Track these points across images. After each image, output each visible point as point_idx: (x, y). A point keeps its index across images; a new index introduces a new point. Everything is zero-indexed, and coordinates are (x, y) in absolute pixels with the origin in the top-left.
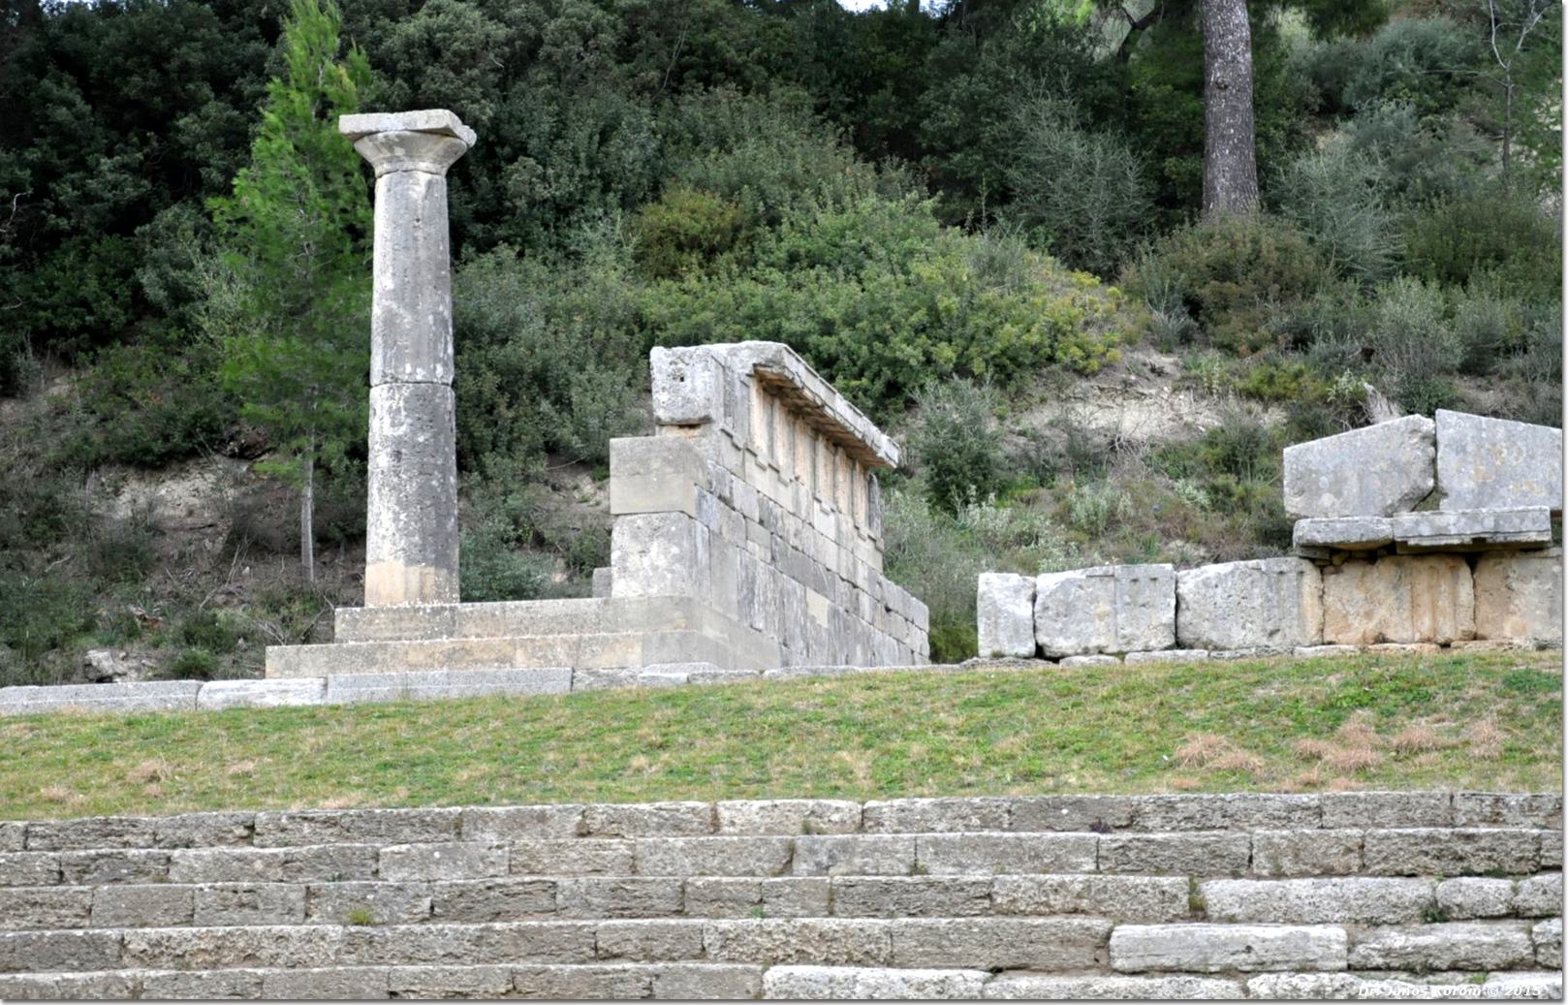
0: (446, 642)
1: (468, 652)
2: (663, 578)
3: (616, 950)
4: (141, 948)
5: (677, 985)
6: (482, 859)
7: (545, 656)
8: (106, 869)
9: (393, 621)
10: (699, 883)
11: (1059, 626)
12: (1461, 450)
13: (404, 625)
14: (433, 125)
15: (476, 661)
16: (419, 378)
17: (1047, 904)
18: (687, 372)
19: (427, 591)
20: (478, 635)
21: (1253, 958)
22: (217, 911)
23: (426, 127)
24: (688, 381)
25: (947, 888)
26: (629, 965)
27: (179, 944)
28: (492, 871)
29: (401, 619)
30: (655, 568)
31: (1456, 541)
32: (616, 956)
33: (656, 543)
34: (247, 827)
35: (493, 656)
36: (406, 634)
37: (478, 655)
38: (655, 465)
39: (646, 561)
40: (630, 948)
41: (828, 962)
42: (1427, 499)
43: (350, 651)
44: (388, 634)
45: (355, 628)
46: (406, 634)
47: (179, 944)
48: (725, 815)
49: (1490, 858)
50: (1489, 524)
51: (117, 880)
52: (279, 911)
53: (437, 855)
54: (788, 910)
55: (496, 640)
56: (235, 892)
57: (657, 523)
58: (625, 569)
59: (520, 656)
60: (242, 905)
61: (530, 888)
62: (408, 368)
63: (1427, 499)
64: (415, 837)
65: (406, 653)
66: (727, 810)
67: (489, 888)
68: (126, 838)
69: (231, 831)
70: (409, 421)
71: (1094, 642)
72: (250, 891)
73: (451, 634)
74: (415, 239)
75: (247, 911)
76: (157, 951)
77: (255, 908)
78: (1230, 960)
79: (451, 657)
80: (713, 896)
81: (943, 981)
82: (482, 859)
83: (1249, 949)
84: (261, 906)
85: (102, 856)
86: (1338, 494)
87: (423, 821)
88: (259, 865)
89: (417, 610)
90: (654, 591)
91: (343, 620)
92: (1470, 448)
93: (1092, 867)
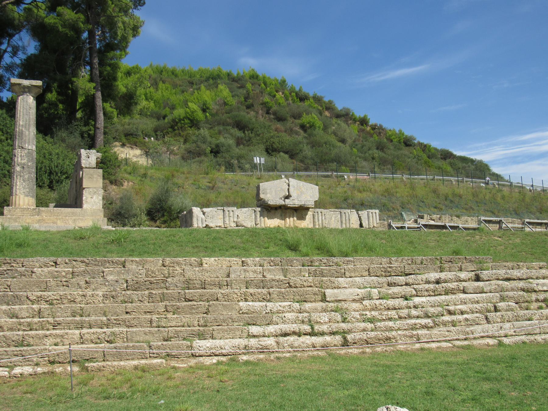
0: (37, 217)
1: (44, 220)
2: (97, 204)
3: (191, 299)
4: (34, 298)
5: (216, 308)
6: (137, 273)
7: (66, 223)
8: (10, 274)
9: (21, 211)
10: (209, 280)
11: (211, 220)
12: (294, 187)
13: (25, 212)
14: (37, 84)
15: (47, 223)
16: (29, 148)
17: (304, 285)
18: (90, 156)
19: (30, 204)
20: (46, 216)
21: (359, 297)
22: (55, 287)
23: (36, 84)
24: (90, 158)
25: (278, 281)
26: (195, 303)
27: (48, 297)
28: (140, 276)
29: (24, 211)
30: (95, 202)
31: (297, 206)
32: (191, 301)
33: (95, 196)
34: (54, 263)
35: (51, 222)
36: (26, 215)
37: (46, 221)
38: (95, 176)
39: (92, 200)
40: (195, 298)
41: (253, 301)
42: (288, 197)
43: (9, 218)
44: (20, 215)
45: (10, 212)
46: (26, 215)
47: (48, 297)
48: (204, 261)
49: (395, 272)
50: (303, 203)
51: (14, 278)
52: (76, 287)
53: (123, 271)
54: (235, 287)
55: (52, 218)
56: (61, 282)
57: (95, 191)
58: (87, 202)
59: (59, 222)
60: (63, 286)
61: (158, 281)
62: (27, 145)
63: (288, 197)
64: (111, 266)
65: (26, 220)
66: (205, 260)
67: (145, 281)
68: (12, 264)
69: (49, 263)
70: (26, 159)
71: (218, 225)
72: (66, 281)
73: (38, 215)
74: (29, 113)
75: (65, 287)
76: (40, 299)
77: (68, 287)
78: (354, 297)
79: (39, 221)
80: (213, 284)
81: (290, 305)
82: (137, 273)
83: (358, 295)
84: (70, 286)
85: (9, 270)
86: (271, 194)
87: (113, 262)
88: (64, 274)
89: (29, 208)
90: (94, 208)
91: (7, 210)
92: (296, 187)
93: (308, 275)
